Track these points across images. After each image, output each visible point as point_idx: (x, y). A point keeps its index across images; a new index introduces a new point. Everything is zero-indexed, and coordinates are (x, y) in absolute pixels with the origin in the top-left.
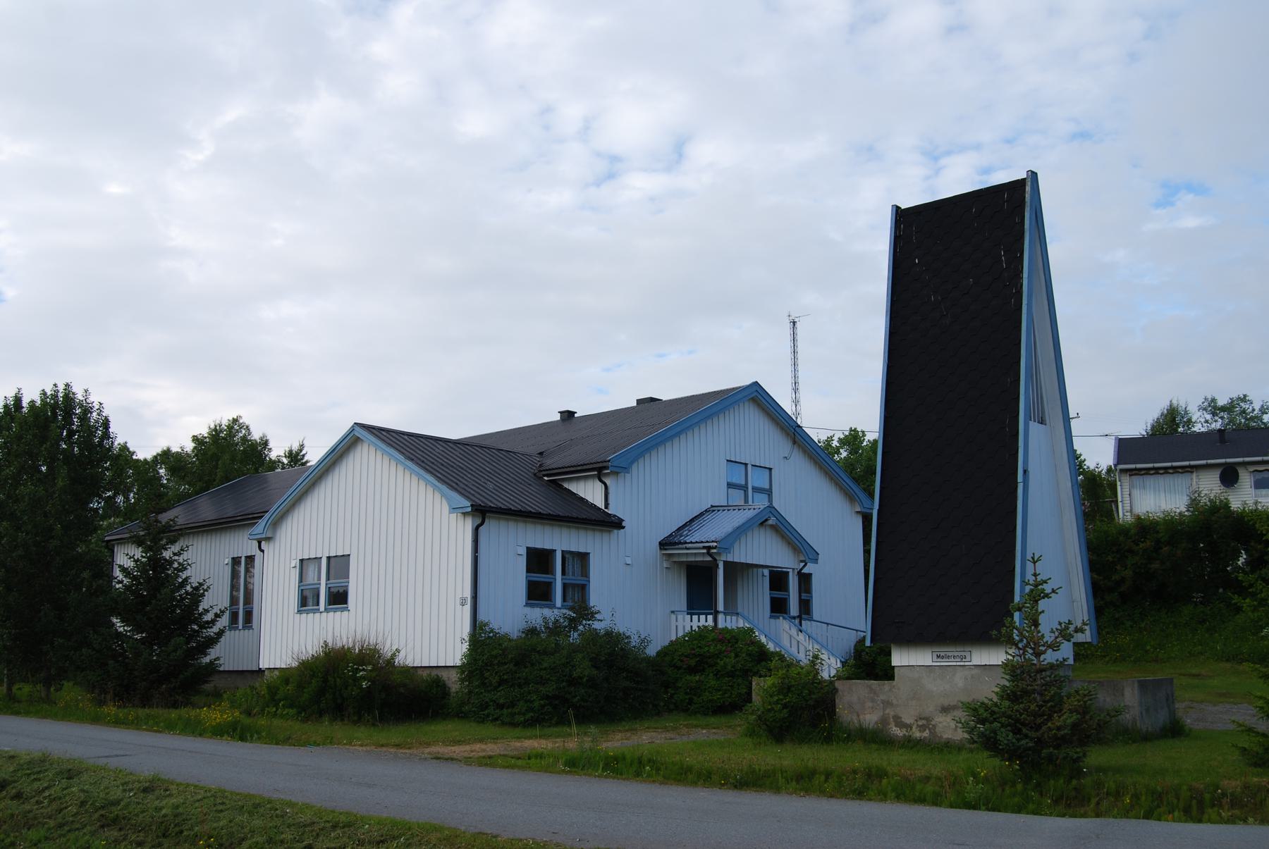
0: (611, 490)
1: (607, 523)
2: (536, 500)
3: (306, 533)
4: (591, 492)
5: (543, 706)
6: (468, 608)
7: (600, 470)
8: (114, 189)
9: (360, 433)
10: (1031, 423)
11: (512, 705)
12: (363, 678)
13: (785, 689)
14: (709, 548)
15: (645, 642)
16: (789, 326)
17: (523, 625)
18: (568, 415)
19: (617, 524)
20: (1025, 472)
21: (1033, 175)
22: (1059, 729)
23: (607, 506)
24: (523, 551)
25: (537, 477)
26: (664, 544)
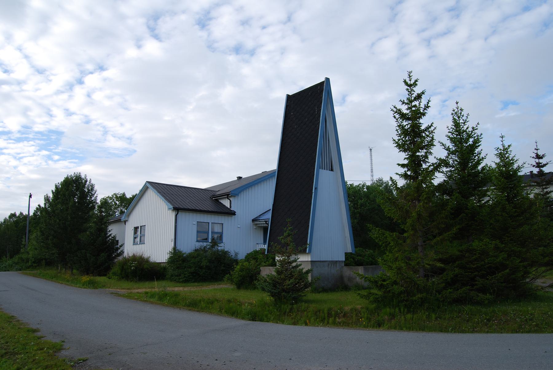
0: (232, 202)
1: (230, 213)
2: (209, 206)
3: (136, 218)
4: (226, 203)
5: (189, 276)
6: (173, 242)
7: (228, 195)
8: (166, 118)
9: (148, 185)
10: (321, 170)
11: (180, 275)
12: (133, 266)
13: (241, 270)
14: (266, 221)
15: (236, 254)
16: (369, 152)
17: (194, 248)
18: (240, 178)
19: (233, 213)
20: (316, 188)
21: (328, 80)
22: (289, 285)
23: (231, 207)
24: (195, 223)
25: (211, 198)
26: (253, 220)
